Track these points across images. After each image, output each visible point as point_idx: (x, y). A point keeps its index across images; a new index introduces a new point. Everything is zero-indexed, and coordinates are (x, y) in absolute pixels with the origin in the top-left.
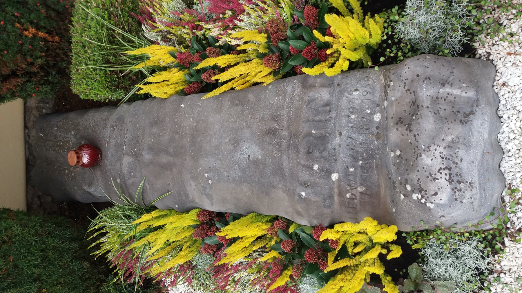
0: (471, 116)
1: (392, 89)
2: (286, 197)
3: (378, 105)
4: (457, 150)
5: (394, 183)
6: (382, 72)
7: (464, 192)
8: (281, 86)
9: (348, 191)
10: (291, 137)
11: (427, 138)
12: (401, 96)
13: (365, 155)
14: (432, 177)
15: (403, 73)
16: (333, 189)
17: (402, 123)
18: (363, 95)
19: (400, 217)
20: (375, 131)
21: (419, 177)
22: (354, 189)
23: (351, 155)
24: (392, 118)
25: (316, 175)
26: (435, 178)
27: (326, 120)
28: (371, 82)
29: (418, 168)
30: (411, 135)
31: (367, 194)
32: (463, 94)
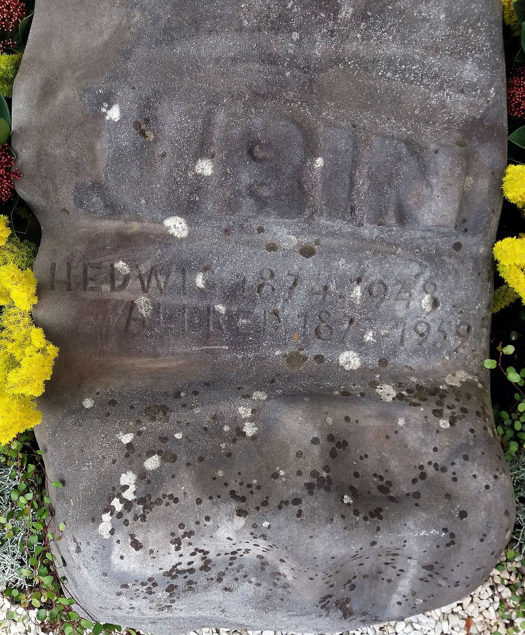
0: (340, 613)
1: (428, 425)
2: (98, 41)
3: (383, 362)
4: (253, 580)
5: (165, 410)
6: (477, 374)
7: (145, 598)
8: (482, 38)
9: (133, 264)
10: (306, 69)
11: (291, 538)
12: (406, 446)
13: (244, 321)
14: (183, 537)
15: (473, 468)
16: (139, 219)
17: (333, 454)
18: (419, 323)
19: (69, 422)
20: (310, 353)
21: (182, 502)
22: (142, 283)
23: (244, 281)
24: (347, 419)
25: (177, 166)
26: (180, 544)
27: (353, 209)
28: (452, 342)
29: (206, 502)
30: (298, 491)
31: (128, 322)
32: (396, 598)
